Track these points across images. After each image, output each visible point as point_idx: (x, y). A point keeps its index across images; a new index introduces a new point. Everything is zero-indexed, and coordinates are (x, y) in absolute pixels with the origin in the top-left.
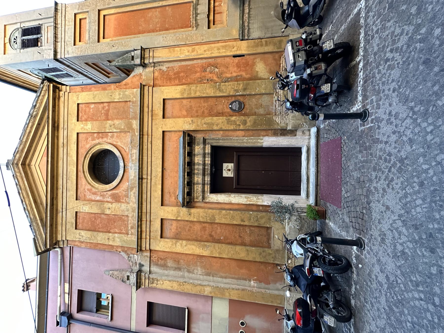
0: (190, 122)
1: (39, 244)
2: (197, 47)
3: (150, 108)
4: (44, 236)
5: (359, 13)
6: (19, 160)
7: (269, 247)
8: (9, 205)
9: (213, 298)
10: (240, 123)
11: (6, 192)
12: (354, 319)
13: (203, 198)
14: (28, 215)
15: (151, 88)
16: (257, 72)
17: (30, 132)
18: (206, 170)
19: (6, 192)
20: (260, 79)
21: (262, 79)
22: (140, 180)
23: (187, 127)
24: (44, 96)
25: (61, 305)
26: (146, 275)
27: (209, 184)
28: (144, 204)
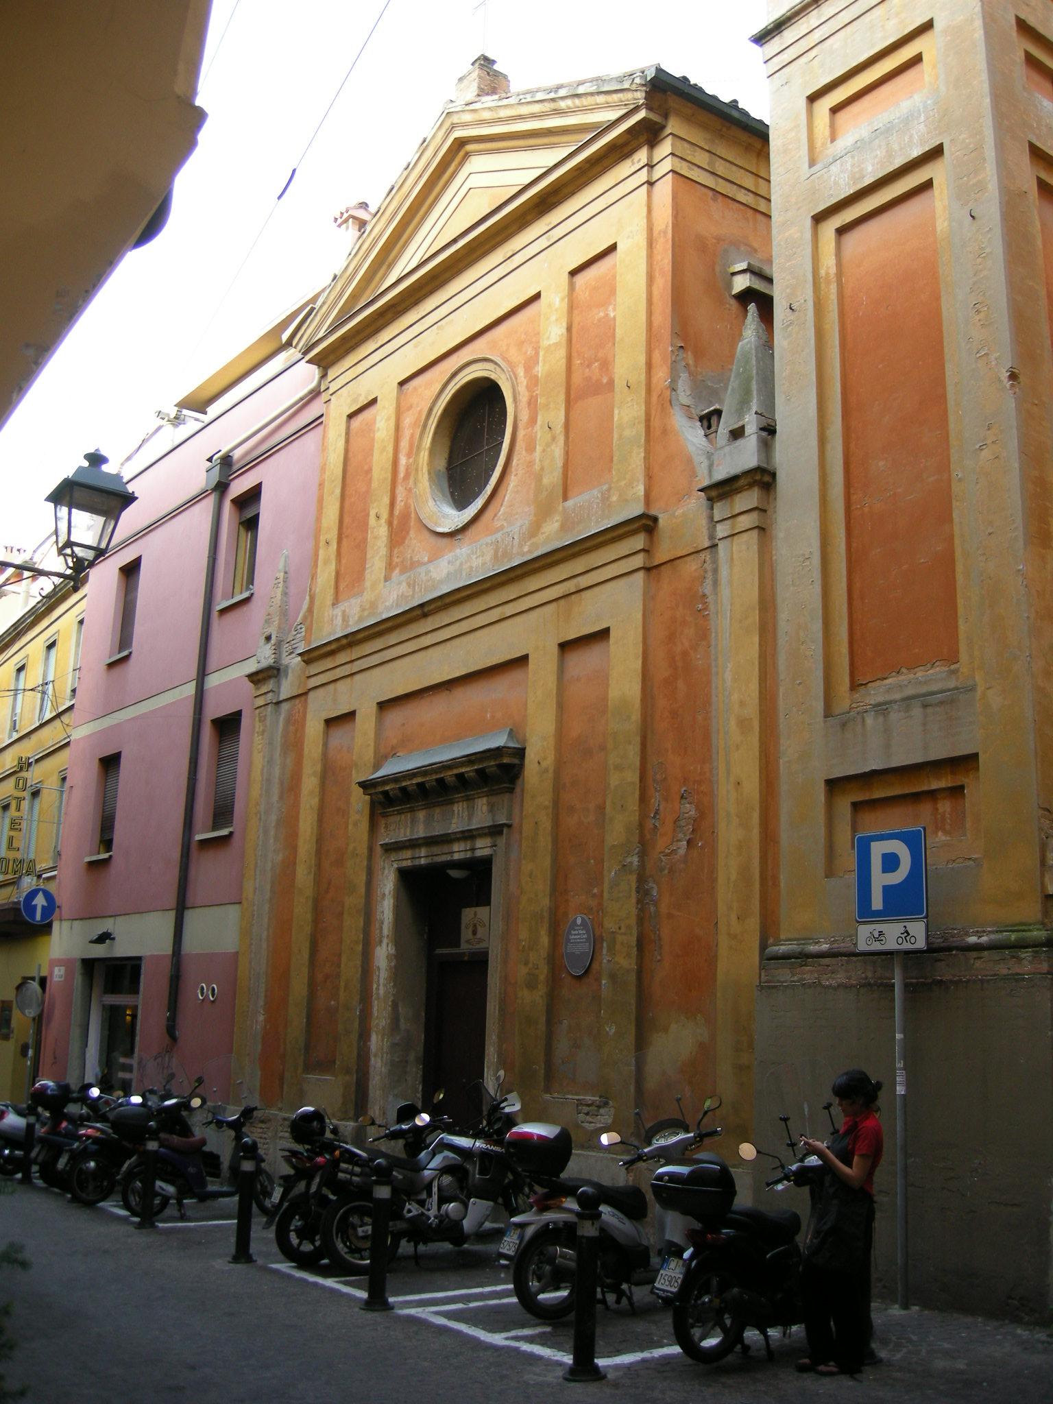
0: (544, 764)
1: (305, 331)
2: (754, 739)
3: (584, 581)
4: (321, 335)
5: (449, 1315)
6: (465, 125)
7: (308, 1068)
8: (279, 198)
9: (237, 907)
10: (530, 965)
11: (294, 171)
12: (41, 1189)
13: (390, 848)
14: (353, 253)
15: (638, 561)
16: (666, 1030)
17: (521, 118)
18: (445, 849)
19: (294, 171)
20: (641, 1043)
21: (549, 1022)
22: (419, 612)
23: (531, 756)
24: (609, 106)
25: (653, 413)
26: (271, 694)
27: (417, 862)
28: (378, 644)
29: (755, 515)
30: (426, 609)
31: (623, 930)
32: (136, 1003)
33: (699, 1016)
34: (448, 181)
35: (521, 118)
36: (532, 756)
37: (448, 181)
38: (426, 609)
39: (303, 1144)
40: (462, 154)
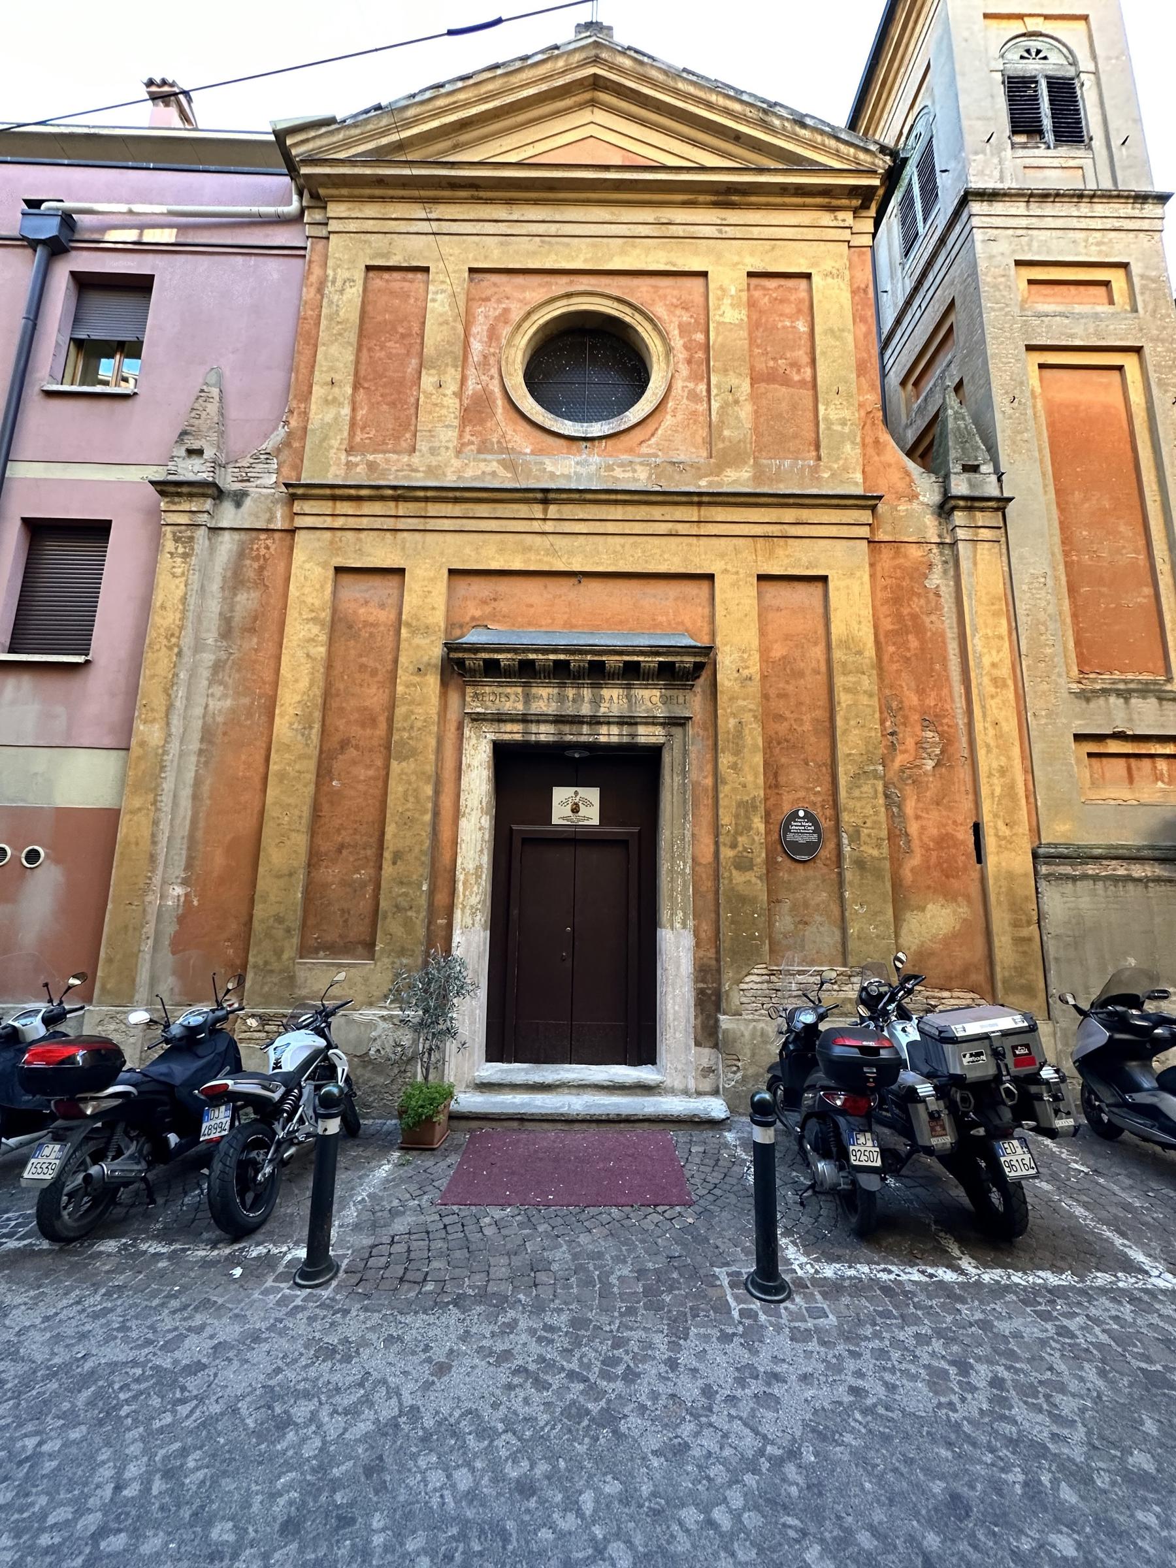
7: (304, 951)
10: (740, 848)
13: (477, 718)
15: (864, 532)
16: (923, 909)
17: (709, 106)
18: (575, 729)
20: (898, 920)
22: (539, 496)
24: (838, 155)
26: (206, 515)
29: (867, 528)
30: (551, 496)
31: (869, 824)
32: (94, 1001)
33: (960, 899)
34: (486, 137)
35: (709, 106)
36: (727, 662)
37: (486, 137)
38: (551, 496)
39: (777, 1221)
40: (587, 96)
